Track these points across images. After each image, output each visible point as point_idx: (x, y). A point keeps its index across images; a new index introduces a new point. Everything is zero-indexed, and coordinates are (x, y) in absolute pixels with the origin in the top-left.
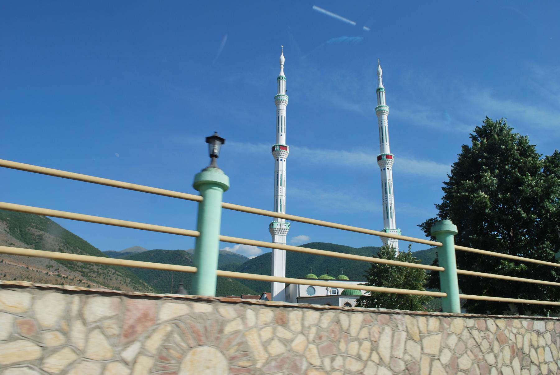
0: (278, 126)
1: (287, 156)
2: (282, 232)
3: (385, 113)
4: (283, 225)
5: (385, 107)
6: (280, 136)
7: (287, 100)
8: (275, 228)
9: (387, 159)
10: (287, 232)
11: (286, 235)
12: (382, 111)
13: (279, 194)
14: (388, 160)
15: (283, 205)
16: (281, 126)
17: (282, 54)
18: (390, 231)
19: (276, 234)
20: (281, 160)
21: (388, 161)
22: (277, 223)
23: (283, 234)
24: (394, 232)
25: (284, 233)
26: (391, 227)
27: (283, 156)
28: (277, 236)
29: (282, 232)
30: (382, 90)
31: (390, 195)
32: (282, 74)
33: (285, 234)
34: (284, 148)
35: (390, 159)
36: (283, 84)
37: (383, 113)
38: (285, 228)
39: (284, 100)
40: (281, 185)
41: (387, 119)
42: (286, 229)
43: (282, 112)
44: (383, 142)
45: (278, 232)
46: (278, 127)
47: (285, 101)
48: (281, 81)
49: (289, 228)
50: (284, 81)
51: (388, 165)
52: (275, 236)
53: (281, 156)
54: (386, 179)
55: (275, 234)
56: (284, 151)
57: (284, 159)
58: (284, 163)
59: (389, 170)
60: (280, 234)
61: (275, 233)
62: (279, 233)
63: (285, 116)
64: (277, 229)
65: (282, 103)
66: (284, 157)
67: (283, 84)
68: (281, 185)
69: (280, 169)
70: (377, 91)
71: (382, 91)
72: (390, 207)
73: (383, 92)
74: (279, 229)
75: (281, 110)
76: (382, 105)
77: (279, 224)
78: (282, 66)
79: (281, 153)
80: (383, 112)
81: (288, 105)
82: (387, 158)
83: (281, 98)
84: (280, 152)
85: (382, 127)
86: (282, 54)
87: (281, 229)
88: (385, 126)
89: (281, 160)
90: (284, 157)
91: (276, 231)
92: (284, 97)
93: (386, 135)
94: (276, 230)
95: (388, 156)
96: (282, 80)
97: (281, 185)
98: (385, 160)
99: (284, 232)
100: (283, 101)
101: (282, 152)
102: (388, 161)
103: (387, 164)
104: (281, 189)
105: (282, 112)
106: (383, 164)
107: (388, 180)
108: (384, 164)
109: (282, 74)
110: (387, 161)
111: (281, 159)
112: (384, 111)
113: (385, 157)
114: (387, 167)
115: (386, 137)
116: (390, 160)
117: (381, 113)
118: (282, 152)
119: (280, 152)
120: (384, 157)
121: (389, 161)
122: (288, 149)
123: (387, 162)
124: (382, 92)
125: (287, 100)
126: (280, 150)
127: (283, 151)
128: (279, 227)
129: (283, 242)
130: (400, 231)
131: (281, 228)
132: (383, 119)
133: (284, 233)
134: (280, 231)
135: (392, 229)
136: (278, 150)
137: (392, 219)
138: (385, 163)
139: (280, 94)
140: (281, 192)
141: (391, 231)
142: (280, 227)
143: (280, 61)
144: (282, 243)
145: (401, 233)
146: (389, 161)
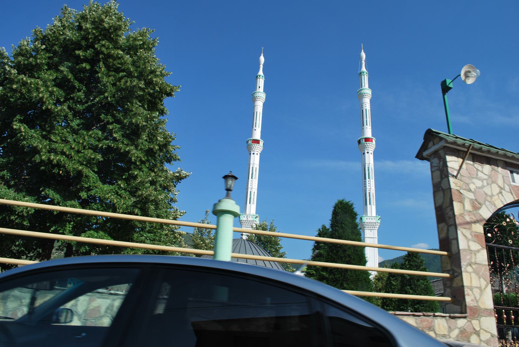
0: (363, 119)
1: (374, 149)
2: (369, 226)
3: (366, 96)
4: (249, 217)
5: (368, 90)
6: (254, 131)
7: (370, 93)
8: (365, 223)
9: (366, 142)
10: (377, 226)
11: (377, 229)
12: (363, 94)
13: (368, 187)
14: (367, 144)
15: (252, 197)
16: (255, 121)
17: (363, 50)
18: (367, 219)
19: (366, 228)
20: (368, 153)
21: (367, 145)
22: (244, 216)
23: (374, 229)
24: (369, 219)
25: (374, 228)
26: (369, 214)
27: (255, 150)
28: (368, 230)
29: (369, 226)
30: (364, 73)
31: (369, 180)
32: (364, 69)
33: (376, 228)
34: (257, 142)
35: (369, 142)
36: (261, 82)
37: (364, 96)
38: (252, 220)
39: (259, 97)
40: (369, 178)
41: (369, 102)
42: (253, 221)
43: (366, 106)
44: (363, 126)
45: (245, 224)
46: (363, 121)
47: (260, 98)
48: (363, 76)
49: (379, 221)
50: (261, 79)
51: (368, 149)
52: (365, 230)
53: (253, 150)
54: (365, 164)
55: (365, 229)
56: (255, 144)
57: (370, 152)
58: (258, 156)
59: (368, 154)
60: (247, 226)
61: (365, 227)
62: (369, 227)
63: (369, 109)
64: (244, 221)
65: (257, 100)
66: (371, 149)
67: (261, 82)
68: (369, 178)
69: (367, 162)
70: (359, 75)
71: (363, 74)
72: (369, 192)
73: (365, 76)
74: (246, 221)
75: (256, 107)
76: (363, 87)
77: (246, 216)
78: (363, 62)
79: (253, 147)
80: (364, 95)
81: (264, 102)
82: (365, 141)
83: (256, 95)
84: (252, 146)
85: (363, 111)
86: (363, 50)
87: (247, 221)
88: (366, 110)
89: (368, 153)
90: (371, 149)
91: (366, 225)
92: (261, 94)
93: (366, 118)
94: (243, 222)
95: (367, 140)
96: (259, 78)
97: (252, 178)
98: (364, 144)
99: (375, 226)
100: (258, 97)
101: (253, 146)
102: (367, 145)
103: (367, 148)
104: (252, 182)
105: (366, 106)
106: (362, 148)
107: (367, 165)
108: (363, 148)
109: (364, 69)
110: (365, 145)
111: (254, 152)
112: (365, 94)
113: (364, 140)
114: (366, 151)
115: (366, 120)
116: (369, 143)
117: (362, 96)
118: (253, 146)
119: (252, 146)
120: (362, 140)
121: (368, 144)
122: (374, 141)
123: (366, 146)
124: (364, 75)
125: (265, 97)
126: (252, 144)
127: (254, 145)
128: (245, 219)
129: (375, 237)
130: (379, 218)
131: (248, 220)
132: (364, 102)
133: (374, 228)
134: (247, 223)
135: (371, 216)
136: (250, 144)
137: (370, 206)
138: (364, 147)
139: (362, 88)
140: (251, 184)
141: (368, 219)
142: (246, 219)
143: (360, 58)
144: (374, 238)
145: (380, 220)
146: (368, 144)
